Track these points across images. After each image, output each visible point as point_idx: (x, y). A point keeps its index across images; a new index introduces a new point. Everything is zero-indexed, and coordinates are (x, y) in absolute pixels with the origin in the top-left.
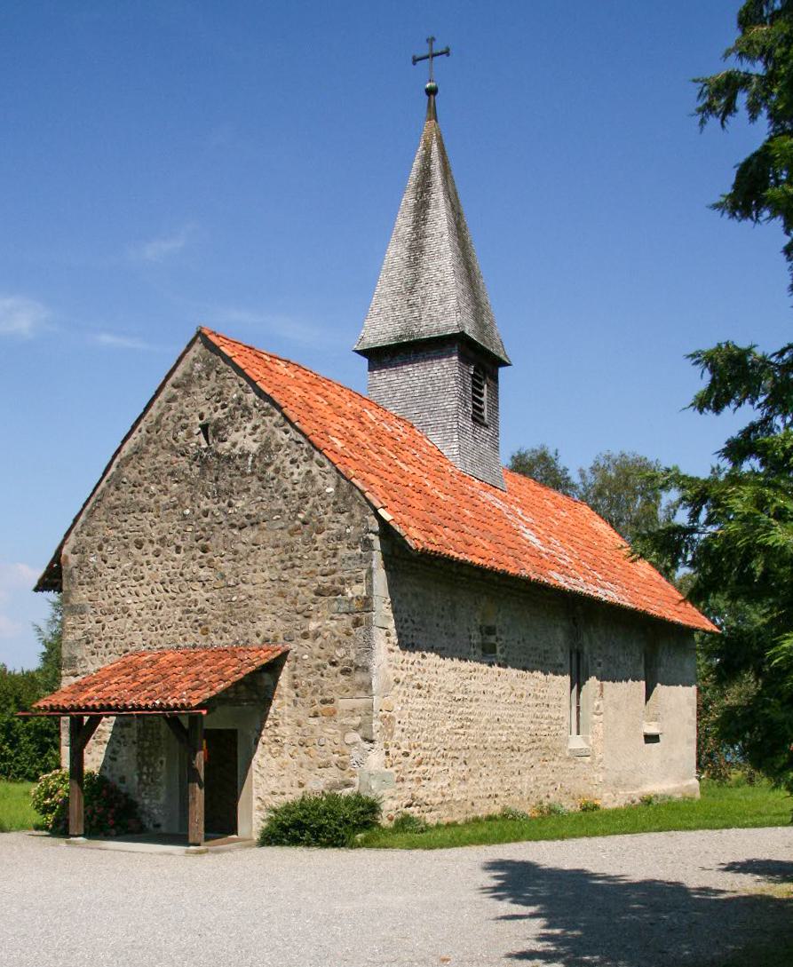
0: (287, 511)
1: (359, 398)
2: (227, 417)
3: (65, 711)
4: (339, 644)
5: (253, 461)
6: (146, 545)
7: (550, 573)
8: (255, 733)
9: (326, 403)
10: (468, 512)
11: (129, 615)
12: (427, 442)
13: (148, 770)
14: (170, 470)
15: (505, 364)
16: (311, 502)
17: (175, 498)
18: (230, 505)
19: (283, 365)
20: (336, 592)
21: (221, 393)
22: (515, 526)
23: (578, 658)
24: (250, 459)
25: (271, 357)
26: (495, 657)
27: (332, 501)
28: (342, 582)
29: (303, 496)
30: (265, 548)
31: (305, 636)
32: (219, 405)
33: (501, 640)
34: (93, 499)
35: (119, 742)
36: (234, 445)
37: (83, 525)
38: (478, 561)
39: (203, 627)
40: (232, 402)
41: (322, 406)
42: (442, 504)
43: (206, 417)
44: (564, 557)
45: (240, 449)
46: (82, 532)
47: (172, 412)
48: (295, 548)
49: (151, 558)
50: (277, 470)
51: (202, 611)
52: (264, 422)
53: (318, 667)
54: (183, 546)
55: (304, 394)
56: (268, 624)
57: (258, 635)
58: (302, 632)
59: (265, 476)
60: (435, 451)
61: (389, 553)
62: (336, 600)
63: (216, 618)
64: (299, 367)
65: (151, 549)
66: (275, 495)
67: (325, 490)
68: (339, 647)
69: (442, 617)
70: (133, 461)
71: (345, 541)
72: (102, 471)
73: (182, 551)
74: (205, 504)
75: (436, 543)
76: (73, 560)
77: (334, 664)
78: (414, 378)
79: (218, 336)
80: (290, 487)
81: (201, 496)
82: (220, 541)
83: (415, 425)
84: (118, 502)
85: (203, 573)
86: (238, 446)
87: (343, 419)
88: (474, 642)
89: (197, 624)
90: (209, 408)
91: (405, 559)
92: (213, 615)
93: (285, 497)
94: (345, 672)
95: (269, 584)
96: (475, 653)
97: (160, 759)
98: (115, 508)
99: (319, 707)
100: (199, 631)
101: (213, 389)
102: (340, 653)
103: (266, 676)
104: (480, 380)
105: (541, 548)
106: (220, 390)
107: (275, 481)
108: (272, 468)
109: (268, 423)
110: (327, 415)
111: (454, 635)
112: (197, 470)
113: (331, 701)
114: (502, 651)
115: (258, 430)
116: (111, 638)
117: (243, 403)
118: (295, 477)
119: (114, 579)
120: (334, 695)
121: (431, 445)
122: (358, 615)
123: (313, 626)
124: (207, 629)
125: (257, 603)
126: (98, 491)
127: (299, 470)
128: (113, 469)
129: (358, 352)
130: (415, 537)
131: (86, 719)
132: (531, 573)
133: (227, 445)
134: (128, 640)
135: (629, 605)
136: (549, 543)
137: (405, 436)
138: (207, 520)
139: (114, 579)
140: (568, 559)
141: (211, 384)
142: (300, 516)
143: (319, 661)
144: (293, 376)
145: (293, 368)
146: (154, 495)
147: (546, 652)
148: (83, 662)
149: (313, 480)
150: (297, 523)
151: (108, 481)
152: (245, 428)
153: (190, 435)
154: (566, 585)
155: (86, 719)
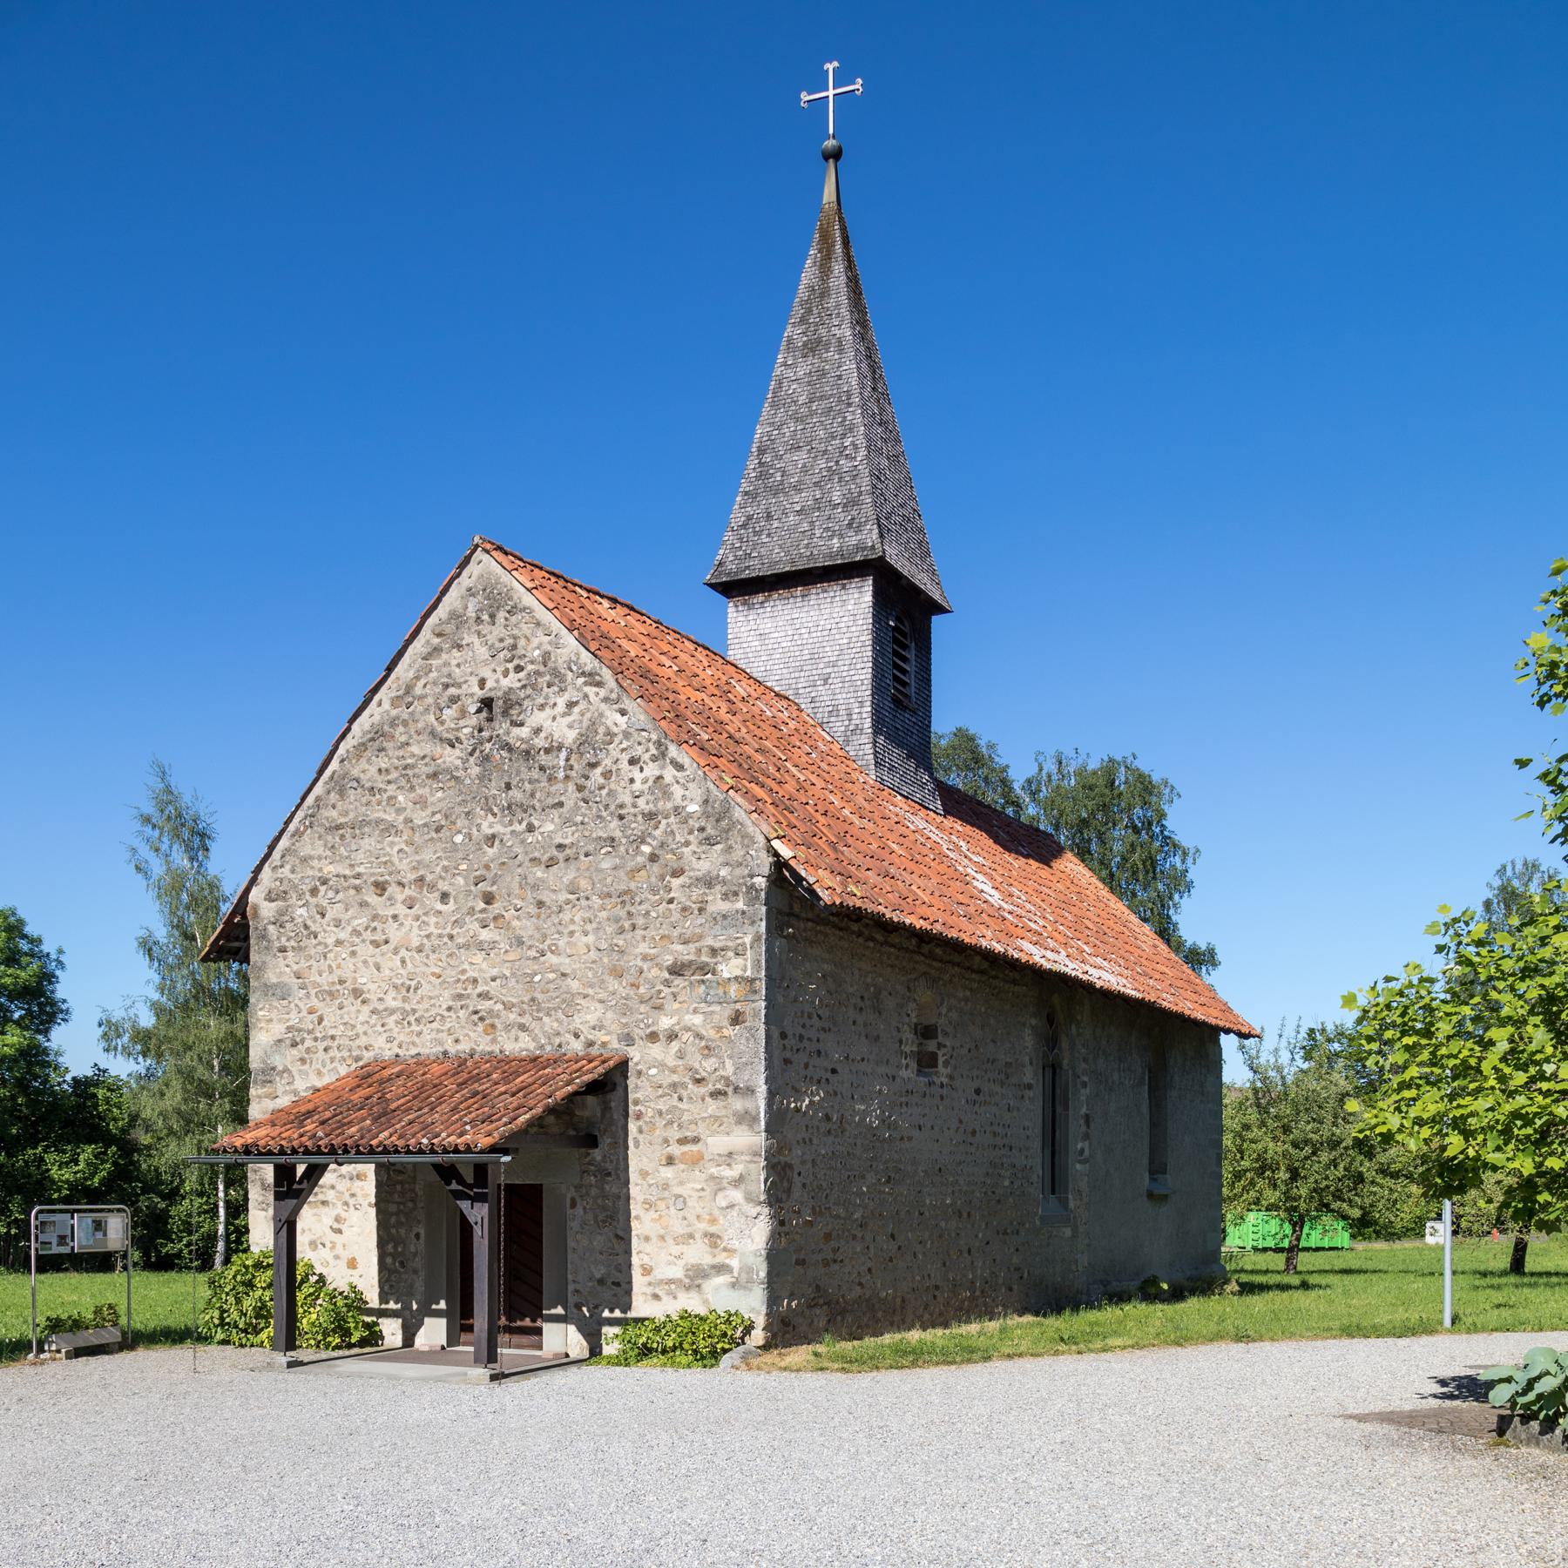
0: (624, 841)
1: (721, 661)
2: (524, 687)
3: (265, 1154)
4: (708, 1050)
5: (567, 760)
6: (392, 889)
7: (1020, 942)
8: (573, 1189)
9: (675, 668)
10: (894, 846)
11: (364, 1002)
12: (823, 733)
13: (395, 1247)
14: (430, 770)
15: (941, 610)
16: (663, 826)
17: (438, 817)
18: (531, 829)
19: (606, 604)
20: (703, 969)
21: (514, 647)
22: (961, 869)
23: (1054, 1073)
24: (563, 754)
25: (589, 591)
26: (936, 1073)
27: (697, 826)
28: (714, 952)
29: (650, 816)
30: (587, 899)
31: (653, 1037)
32: (510, 666)
33: (945, 1046)
34: (300, 814)
35: (346, 1204)
36: (538, 731)
37: (283, 857)
38: (919, 924)
39: (487, 1022)
40: (532, 662)
41: (669, 673)
42: (858, 833)
43: (489, 684)
44: (1036, 918)
45: (546, 738)
46: (282, 866)
47: (434, 675)
48: (638, 899)
49: (401, 910)
50: (607, 775)
51: (484, 996)
52: (586, 696)
53: (674, 1086)
54: (453, 893)
55: (644, 653)
56: (592, 1018)
57: (577, 1036)
58: (648, 1031)
59: (588, 783)
60: (836, 747)
61: (786, 910)
62: (703, 981)
63: (508, 1007)
64: (632, 609)
65: (400, 895)
66: (604, 814)
67: (684, 808)
68: (706, 1057)
69: (861, 1009)
70: (368, 753)
71: (718, 887)
72: (317, 768)
73: (452, 900)
74: (489, 825)
75: (859, 894)
76: (267, 910)
77: (698, 1081)
78: (803, 631)
79: (506, 553)
80: (627, 799)
81: (482, 813)
82: (515, 885)
83: (803, 706)
84: (342, 820)
85: (485, 935)
86: (543, 735)
87: (703, 696)
88: (907, 1049)
89: (476, 1017)
90: (495, 671)
91: (808, 920)
92: (503, 1003)
93: (621, 818)
94: (716, 1094)
95: (593, 954)
96: (907, 1066)
97: (415, 1230)
98: (338, 827)
99: (676, 1150)
100: (481, 1027)
101: (501, 640)
102: (709, 1064)
103: (591, 1100)
104: (904, 635)
105: (1003, 904)
106: (512, 641)
107: (604, 792)
108: (599, 770)
109: (592, 698)
110: (679, 687)
111: (877, 1038)
112: (475, 770)
113: (696, 1140)
114: (946, 1064)
115: (576, 710)
116: (333, 1038)
117: (550, 664)
118: (637, 786)
119: (339, 943)
120: (701, 1130)
121: (829, 739)
122: (738, 1006)
123: (665, 1023)
124: (493, 1026)
125: (575, 985)
126: (310, 800)
127: (643, 775)
128: (334, 765)
129: (712, 586)
130: (828, 887)
131: (301, 1169)
132: (994, 943)
133: (524, 732)
134: (363, 1041)
135: (1133, 993)
136: (1011, 895)
137: (792, 724)
138: (490, 852)
139: (339, 943)
140: (1042, 922)
141: (498, 631)
142: (646, 849)
143: (675, 1078)
144: (623, 624)
145: (621, 610)
146: (405, 809)
147: (1008, 1065)
148: (285, 1075)
149: (667, 795)
150: (640, 859)
151: (326, 783)
152: (555, 704)
153: (463, 713)
154: (1043, 961)
155: (301, 1169)
